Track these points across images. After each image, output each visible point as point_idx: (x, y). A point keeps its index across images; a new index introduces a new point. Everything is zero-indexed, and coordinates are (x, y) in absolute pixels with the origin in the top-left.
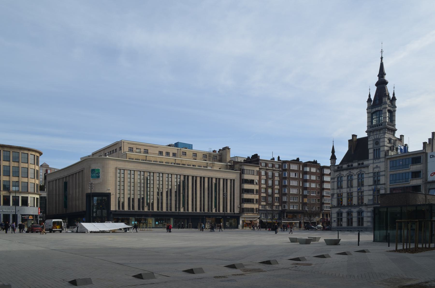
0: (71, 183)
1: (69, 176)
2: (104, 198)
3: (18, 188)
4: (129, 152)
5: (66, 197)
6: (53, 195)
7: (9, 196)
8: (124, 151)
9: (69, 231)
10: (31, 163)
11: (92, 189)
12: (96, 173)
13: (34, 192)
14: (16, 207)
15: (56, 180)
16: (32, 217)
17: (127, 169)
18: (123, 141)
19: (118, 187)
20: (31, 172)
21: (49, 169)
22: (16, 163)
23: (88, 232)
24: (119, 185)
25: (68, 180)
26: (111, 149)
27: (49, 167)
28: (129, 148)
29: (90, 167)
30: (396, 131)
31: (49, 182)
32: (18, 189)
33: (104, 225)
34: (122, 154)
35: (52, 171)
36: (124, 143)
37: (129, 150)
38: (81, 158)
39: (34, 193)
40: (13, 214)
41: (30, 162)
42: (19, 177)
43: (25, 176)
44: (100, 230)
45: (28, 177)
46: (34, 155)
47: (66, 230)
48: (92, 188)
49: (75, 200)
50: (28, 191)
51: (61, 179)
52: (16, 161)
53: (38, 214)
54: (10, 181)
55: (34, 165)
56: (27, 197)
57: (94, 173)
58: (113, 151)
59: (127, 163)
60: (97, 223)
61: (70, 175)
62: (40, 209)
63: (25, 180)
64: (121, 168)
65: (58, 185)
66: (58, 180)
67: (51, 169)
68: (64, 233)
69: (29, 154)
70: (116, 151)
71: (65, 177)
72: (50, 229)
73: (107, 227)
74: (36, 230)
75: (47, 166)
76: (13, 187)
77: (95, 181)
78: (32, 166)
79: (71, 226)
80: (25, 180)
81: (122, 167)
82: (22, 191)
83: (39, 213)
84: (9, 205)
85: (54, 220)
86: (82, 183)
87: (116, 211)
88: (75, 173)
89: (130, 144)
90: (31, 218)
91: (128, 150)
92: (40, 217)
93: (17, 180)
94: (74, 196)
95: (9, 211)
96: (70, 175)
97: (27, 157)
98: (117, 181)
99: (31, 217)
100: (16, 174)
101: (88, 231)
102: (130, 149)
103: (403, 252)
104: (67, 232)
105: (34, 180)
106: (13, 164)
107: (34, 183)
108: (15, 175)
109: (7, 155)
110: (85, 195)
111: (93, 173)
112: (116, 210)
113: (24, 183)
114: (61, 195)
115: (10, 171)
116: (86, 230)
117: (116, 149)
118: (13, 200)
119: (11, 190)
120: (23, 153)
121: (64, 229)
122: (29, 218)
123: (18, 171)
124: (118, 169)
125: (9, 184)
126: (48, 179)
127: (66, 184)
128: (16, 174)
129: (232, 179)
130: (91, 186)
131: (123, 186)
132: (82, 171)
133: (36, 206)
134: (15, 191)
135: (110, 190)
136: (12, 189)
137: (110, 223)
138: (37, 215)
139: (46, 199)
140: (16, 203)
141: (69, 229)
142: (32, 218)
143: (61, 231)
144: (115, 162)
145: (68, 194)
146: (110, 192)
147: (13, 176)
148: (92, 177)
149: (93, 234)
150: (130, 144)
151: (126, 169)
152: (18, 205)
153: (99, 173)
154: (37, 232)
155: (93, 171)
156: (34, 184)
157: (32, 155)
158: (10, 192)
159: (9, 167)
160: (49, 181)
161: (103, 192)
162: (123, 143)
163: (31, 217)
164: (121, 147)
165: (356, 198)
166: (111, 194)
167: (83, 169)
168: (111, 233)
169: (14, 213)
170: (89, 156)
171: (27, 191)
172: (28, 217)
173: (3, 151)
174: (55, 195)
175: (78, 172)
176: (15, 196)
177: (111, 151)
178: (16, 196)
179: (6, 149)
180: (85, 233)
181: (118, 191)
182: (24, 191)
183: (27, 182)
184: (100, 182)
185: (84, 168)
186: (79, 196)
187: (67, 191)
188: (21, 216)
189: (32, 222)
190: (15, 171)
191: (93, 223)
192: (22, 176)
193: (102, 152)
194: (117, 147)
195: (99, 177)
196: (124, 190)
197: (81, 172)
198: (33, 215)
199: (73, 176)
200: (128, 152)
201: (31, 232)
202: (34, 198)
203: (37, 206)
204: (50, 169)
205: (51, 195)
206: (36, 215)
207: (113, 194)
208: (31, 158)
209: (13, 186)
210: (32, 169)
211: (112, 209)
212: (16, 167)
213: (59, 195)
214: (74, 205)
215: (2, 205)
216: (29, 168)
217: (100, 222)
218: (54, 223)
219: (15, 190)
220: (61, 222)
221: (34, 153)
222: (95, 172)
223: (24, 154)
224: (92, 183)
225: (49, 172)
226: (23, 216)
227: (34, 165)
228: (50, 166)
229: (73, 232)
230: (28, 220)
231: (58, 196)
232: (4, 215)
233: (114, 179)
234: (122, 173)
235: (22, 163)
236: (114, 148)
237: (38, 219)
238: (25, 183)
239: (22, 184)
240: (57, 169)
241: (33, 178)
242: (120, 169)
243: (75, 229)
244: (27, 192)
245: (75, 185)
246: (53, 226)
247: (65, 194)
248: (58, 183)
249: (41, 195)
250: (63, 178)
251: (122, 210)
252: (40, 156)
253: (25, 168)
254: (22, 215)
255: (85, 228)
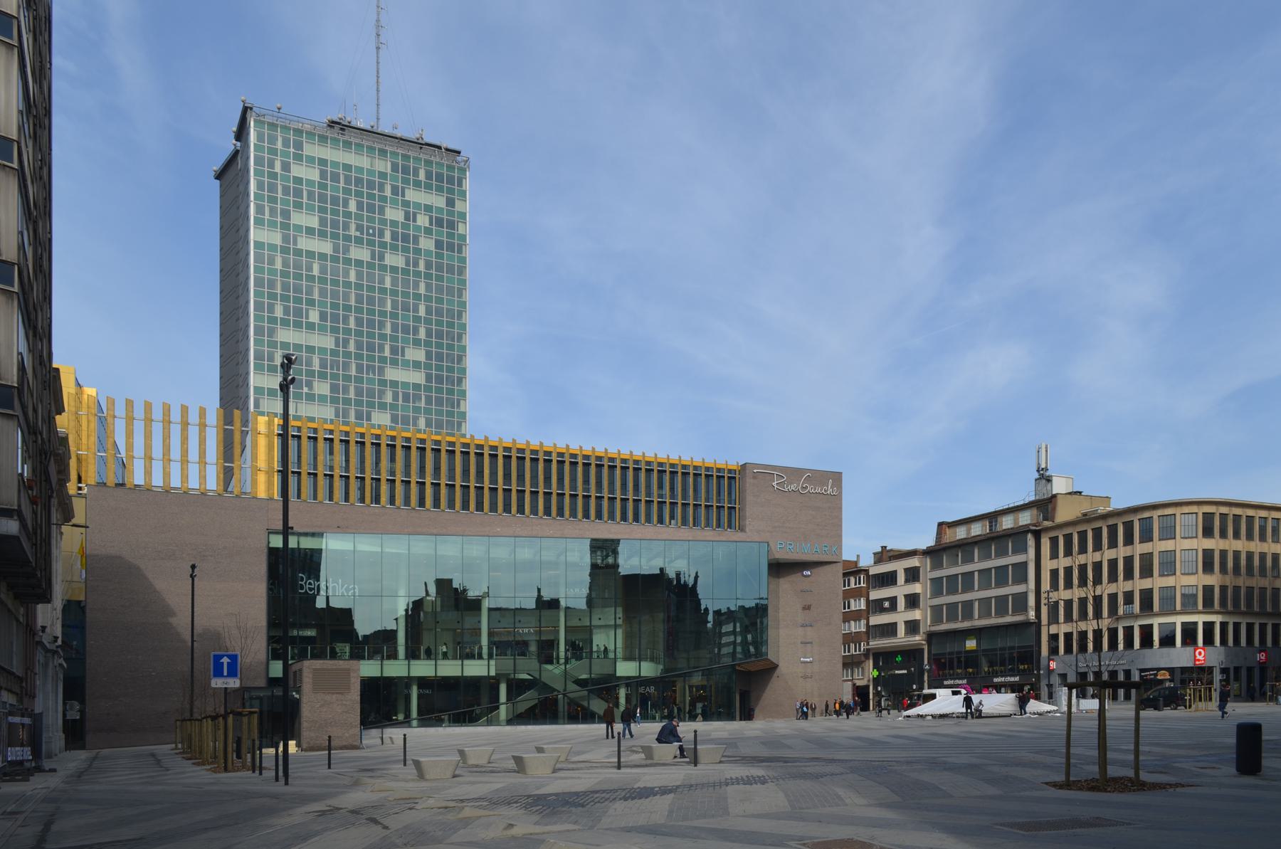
50: (1175, 610)
62: (235, 691)
99: (1164, 674)
103: (1144, 790)
129: (478, 659)
163: (1164, 674)
165: (494, 667)
171: (1173, 608)
172: (1156, 675)
190: (1165, 561)
254: (1142, 670)
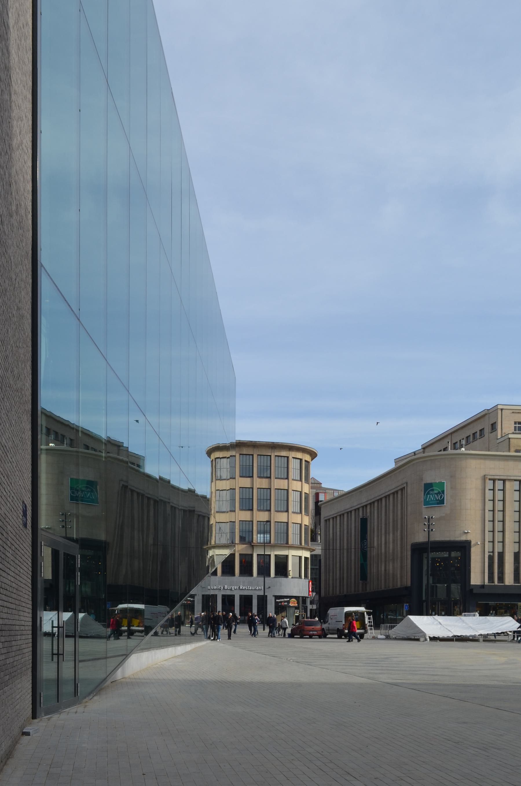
0: (376, 521)
1: (370, 504)
2: (453, 554)
3: (268, 536)
4: (516, 433)
5: (364, 554)
6: (336, 549)
7: (252, 555)
8: (503, 432)
9: (380, 636)
10: (295, 478)
11: (431, 533)
12: (436, 492)
13: (301, 543)
14: (266, 578)
15: (342, 515)
16: (296, 602)
17: (512, 478)
18: (500, 407)
19: (488, 526)
20: (294, 498)
21: (321, 491)
22: (264, 480)
23: (426, 640)
24: (492, 520)
25: (368, 514)
26: (469, 432)
27: (321, 487)
28: (515, 423)
29: (422, 479)
30: (171, 483)
31: (326, 521)
32: (268, 539)
33: (463, 621)
34: (498, 441)
35: (328, 498)
36: (503, 411)
37: (515, 430)
38: (397, 461)
39: (300, 547)
40: (258, 596)
41: (291, 476)
42: (270, 510)
43: (282, 510)
44: (455, 634)
45: (287, 511)
46: (301, 460)
47: (371, 632)
48: (432, 530)
49: (386, 561)
50: (287, 543)
51: (353, 513)
52: (265, 476)
53: (307, 595)
54: (252, 521)
55: (299, 483)
56: (287, 557)
57: (432, 492)
58: (474, 434)
59: (511, 464)
60: (438, 615)
61: (372, 501)
63: (282, 517)
64: (498, 477)
65: (345, 527)
66: (346, 515)
67: (325, 491)
68: (368, 639)
69: (290, 458)
70: (481, 435)
71: (363, 507)
72: (338, 629)
73: (471, 627)
74: (310, 631)
75: (318, 485)
76: (259, 535)
77: (436, 513)
78: (296, 485)
79: (383, 624)
80: (282, 517)
81: (498, 474)
82: (276, 542)
83: (309, 591)
84: (251, 575)
85: (347, 609)
86: (402, 518)
87: (483, 586)
88: (386, 497)
89: (519, 413)
90: (293, 603)
91: (513, 428)
92: (312, 603)
93: (249, 519)
94: (383, 551)
95: (250, 588)
96: (374, 502)
97: (286, 466)
98: (487, 511)
100: (265, 504)
101: (424, 635)
102: (517, 425)
104: (374, 638)
105: (299, 516)
106: (260, 483)
107: (300, 524)
108: (262, 508)
109: (248, 464)
110: (409, 547)
111: (428, 493)
112: (483, 584)
113: (279, 524)
114: (353, 550)
115: (253, 499)
116: (421, 634)
117: (482, 431)
118: (258, 563)
119: (254, 542)
120: (278, 456)
121: (369, 631)
122: (290, 604)
123: (269, 498)
124: (490, 479)
125: (251, 529)
126: (325, 513)
127: (364, 522)
128: (265, 504)
130: (429, 525)
131: (502, 523)
132: (402, 490)
133: (305, 577)
134: (264, 543)
135: (468, 534)
136: (258, 538)
137: (474, 615)
138: (306, 597)
139: (320, 560)
140: (264, 571)
141: (379, 631)
142: (297, 605)
143: (362, 636)
144: (482, 461)
145: (369, 546)
146: (468, 539)
147: (259, 510)
148: (426, 503)
149: (439, 643)
150: (519, 413)
151: (509, 478)
152: (269, 575)
153: (443, 492)
154: (311, 637)
155: (428, 487)
156: (299, 525)
157: (297, 460)
158: (253, 546)
159: (251, 490)
160: (326, 519)
161: (452, 539)
162: (500, 412)
163: (294, 602)
164: (495, 423)
166: (472, 543)
167: (405, 485)
168: (482, 644)
169: (262, 593)
170: (415, 453)
171: (285, 542)
172: (288, 602)
173: (240, 454)
174: (340, 549)
175: (393, 493)
176: (264, 555)
177: (470, 436)
178: (266, 554)
179: (245, 451)
180: (418, 640)
181: (488, 536)
182: (279, 542)
183: (286, 521)
184: (444, 515)
185: (407, 483)
186: (393, 550)
187: (367, 540)
188: (273, 599)
189: (297, 613)
190: (262, 498)
191: (436, 617)
192: (277, 509)
193: (446, 440)
194: (486, 425)
195: (442, 502)
196: (503, 532)
197: (400, 493)
198: (297, 598)
199: (381, 503)
200: (513, 433)
201: (299, 636)
202: (300, 557)
203: (306, 576)
204: (323, 491)
205: (331, 551)
206: (303, 597)
207: (477, 543)
208: (294, 465)
209: (259, 532)
210: (297, 492)
211: (473, 582)
212: (264, 488)
213: (348, 549)
214: (383, 572)
215: (238, 575)
216: (290, 491)
217: (443, 613)
218: (348, 615)
219: (262, 541)
220: (362, 614)
221: (299, 455)
222: (433, 490)
223: (280, 458)
224: (432, 518)
225: (322, 497)
226: (277, 600)
227: (301, 482)
228: (323, 486)
229: (388, 637)
230: (287, 609)
231: (345, 551)
232: (223, 596)
233: (479, 505)
234: (499, 490)
235: (276, 478)
236: (477, 428)
237: (307, 607)
238: (282, 524)
239: (276, 526)
240: (339, 490)
241: (297, 513)
242: (494, 480)
243: (393, 630)
244: (287, 546)
245: (386, 524)
246: (345, 622)
247: (361, 546)
248: (345, 523)
249: (314, 550)
250: (358, 509)
251: (498, 583)
252: (312, 460)
253: (283, 491)
254: (277, 597)
255: (418, 628)
